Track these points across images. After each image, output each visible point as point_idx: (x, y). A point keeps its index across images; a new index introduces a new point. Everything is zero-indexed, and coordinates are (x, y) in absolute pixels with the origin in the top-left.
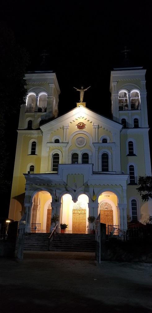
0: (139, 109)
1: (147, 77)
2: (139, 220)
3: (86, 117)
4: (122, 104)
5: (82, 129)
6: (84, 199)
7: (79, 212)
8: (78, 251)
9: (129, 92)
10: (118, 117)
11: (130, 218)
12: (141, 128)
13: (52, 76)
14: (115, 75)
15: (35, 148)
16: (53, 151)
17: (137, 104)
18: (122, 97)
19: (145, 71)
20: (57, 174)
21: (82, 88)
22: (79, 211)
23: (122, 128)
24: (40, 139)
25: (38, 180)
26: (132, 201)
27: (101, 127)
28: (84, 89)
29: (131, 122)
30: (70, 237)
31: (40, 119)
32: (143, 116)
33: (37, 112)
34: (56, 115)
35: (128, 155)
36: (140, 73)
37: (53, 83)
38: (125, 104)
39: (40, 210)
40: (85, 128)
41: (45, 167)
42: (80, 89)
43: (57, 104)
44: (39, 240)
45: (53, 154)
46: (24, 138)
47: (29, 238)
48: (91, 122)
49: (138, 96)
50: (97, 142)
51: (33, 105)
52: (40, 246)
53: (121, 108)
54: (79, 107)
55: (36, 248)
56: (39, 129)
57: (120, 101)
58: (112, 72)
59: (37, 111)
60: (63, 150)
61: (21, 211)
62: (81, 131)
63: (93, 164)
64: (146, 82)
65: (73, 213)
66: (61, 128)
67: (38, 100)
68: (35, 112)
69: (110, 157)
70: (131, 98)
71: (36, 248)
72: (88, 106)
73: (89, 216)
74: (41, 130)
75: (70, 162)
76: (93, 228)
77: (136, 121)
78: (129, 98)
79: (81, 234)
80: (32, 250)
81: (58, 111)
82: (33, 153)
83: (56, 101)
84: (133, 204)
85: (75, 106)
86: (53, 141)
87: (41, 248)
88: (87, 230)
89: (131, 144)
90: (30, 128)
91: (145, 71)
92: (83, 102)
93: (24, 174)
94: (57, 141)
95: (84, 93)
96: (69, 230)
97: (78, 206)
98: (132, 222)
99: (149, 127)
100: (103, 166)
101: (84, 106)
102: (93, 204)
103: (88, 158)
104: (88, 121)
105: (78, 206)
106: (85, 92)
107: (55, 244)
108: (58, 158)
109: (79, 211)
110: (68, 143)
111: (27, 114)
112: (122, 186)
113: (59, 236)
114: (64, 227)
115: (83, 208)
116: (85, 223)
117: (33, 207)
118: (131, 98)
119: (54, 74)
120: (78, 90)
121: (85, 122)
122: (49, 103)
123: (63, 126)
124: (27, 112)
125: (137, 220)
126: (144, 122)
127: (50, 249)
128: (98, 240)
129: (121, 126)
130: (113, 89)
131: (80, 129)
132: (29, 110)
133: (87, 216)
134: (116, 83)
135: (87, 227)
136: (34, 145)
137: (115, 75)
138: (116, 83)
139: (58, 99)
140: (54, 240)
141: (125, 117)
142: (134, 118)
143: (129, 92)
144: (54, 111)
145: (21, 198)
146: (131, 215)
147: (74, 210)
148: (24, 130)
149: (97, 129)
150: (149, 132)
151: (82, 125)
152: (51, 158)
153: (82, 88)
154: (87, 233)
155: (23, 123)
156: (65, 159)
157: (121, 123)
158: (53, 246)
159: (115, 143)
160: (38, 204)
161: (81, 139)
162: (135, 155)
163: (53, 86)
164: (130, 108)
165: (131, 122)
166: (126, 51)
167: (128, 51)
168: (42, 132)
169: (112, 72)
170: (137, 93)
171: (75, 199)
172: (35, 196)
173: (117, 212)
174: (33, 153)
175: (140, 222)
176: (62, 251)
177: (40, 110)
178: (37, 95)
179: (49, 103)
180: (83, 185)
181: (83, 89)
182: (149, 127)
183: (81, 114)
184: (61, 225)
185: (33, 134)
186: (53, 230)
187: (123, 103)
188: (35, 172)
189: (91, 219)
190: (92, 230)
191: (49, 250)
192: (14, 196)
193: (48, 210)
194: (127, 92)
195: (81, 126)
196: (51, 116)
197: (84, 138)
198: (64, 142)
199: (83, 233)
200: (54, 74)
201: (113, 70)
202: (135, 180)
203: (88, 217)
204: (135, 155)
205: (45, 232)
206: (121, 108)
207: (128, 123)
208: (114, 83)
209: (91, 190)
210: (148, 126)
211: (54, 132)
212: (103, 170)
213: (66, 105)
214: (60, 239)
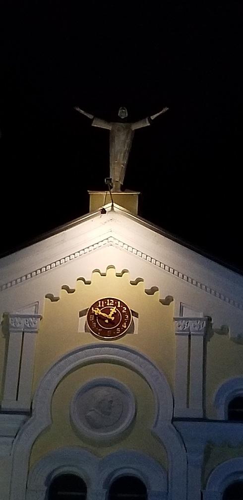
42: (112, 118)
121: (132, 298)
151: (113, 310)
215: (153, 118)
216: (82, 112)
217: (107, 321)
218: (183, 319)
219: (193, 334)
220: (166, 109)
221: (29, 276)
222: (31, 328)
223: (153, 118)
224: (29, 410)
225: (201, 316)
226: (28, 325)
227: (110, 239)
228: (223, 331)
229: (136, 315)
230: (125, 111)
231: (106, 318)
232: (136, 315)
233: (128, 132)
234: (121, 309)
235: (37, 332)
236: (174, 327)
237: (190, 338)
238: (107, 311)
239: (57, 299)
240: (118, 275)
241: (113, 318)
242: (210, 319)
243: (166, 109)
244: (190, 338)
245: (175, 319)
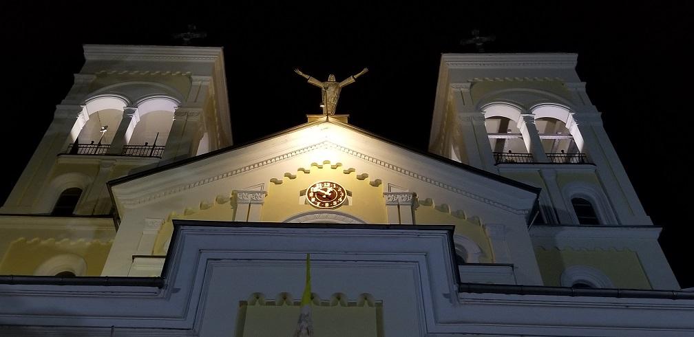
3: (348, 161)
13: (213, 56)
42: (323, 79)
58: (445, 57)
64: (587, 87)
66: (221, 201)
95: (337, 92)
106: (345, 92)
120: (313, 81)
121: (347, 183)
128: (88, 244)
150: (662, 240)
151: (330, 189)
159: (512, 266)
163: (205, 83)
169: (445, 57)
185: (70, 235)
215: (355, 77)
216: (301, 73)
217: (324, 196)
218: (391, 194)
219: (402, 204)
220: (365, 70)
221: (256, 166)
222: (257, 200)
223: (355, 77)
224: (500, 120)
225: (407, 191)
226: (254, 198)
227: (325, 143)
228: (427, 203)
229: (349, 194)
230: (333, 76)
231: (324, 194)
232: (349, 194)
233: (337, 88)
234: (337, 189)
235: (262, 204)
236: (385, 200)
237: (250, 205)
238: (326, 190)
239: (280, 183)
240: (334, 168)
241: (330, 194)
242: (414, 195)
243: (365, 70)
244: (250, 205)
245: (385, 194)
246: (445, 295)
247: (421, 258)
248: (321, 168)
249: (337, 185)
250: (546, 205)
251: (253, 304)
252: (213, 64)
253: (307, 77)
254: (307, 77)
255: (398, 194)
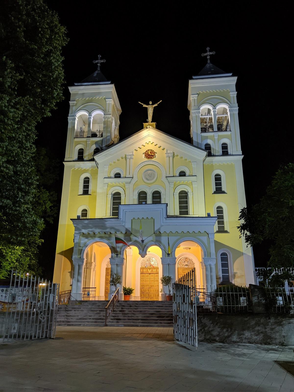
0: (228, 130)
1: (238, 86)
2: (232, 280)
4: (205, 124)
5: (151, 158)
6: (155, 252)
7: (150, 271)
8: (147, 326)
9: (214, 107)
10: (200, 141)
11: (220, 278)
12: (231, 155)
14: (195, 85)
15: (89, 185)
16: (113, 189)
17: (225, 124)
18: (205, 115)
19: (236, 78)
20: (118, 218)
21: (151, 103)
22: (150, 269)
23: (206, 157)
24: (95, 172)
25: (192, 376)
26: (215, 176)
27: (177, 156)
28: (153, 104)
29: (217, 148)
30: (136, 306)
31: (94, 147)
32: (233, 138)
33: (89, 137)
34: (116, 140)
35: (215, 193)
36: (228, 83)
37: (111, 98)
38: (209, 125)
39: (96, 269)
40: (155, 157)
41: (101, 209)
42: (148, 104)
43: (118, 127)
44: (92, 311)
45: (113, 193)
46: (73, 173)
47: (78, 308)
48: (163, 149)
49: (227, 113)
50: (173, 176)
51: (85, 129)
52: (93, 319)
53: (204, 130)
54: (147, 128)
55: (88, 322)
56: (93, 160)
57: (203, 121)
59: (90, 135)
60: (126, 187)
61: (70, 270)
62: (150, 161)
63: (167, 204)
64: (237, 94)
65: (142, 273)
67: (92, 121)
68: (87, 137)
69: (190, 196)
70: (217, 116)
71: (88, 322)
72: (159, 127)
73: (163, 276)
74: (96, 162)
75: (136, 202)
76: (168, 293)
77: (225, 147)
78: (215, 115)
79: (152, 302)
80: (82, 325)
81: (118, 137)
82: (86, 192)
83: (116, 123)
84: (222, 259)
85: (141, 128)
86: (113, 175)
87: (96, 322)
88: (160, 295)
89: (218, 178)
90: (81, 158)
91: (236, 78)
92: (152, 122)
93: (71, 219)
94: (118, 176)
96: (136, 296)
97: (148, 263)
98: (222, 284)
99: (243, 154)
100: (180, 208)
101: (154, 127)
102: (168, 257)
103: (160, 197)
104: (160, 147)
105: (148, 263)
107: (115, 316)
108: (120, 198)
109: (150, 269)
110: (133, 178)
111: (76, 140)
112: (208, 234)
113: (120, 304)
114: (128, 292)
115: (155, 266)
116: (158, 286)
117: (84, 264)
118: (217, 116)
119: (113, 86)
120: (145, 106)
122: (107, 125)
123: (125, 155)
124: (77, 137)
125: (229, 281)
126: (235, 147)
127: (108, 324)
129: (205, 153)
130: (193, 104)
131: (149, 158)
132: (80, 135)
133: (160, 275)
134: (197, 95)
135: (160, 291)
136: (87, 181)
137: (195, 85)
138: (197, 95)
139: (119, 120)
140: (114, 311)
141: (209, 142)
142: (222, 143)
143: (214, 107)
144: (113, 136)
145: (68, 254)
146: (221, 274)
147: (142, 268)
148: (74, 161)
149: (171, 158)
150: (243, 160)
152: (110, 197)
153: (151, 103)
154: (160, 299)
155: (71, 152)
156: (129, 198)
157: (204, 149)
158: (112, 319)
160: (93, 261)
161: (149, 172)
162: (224, 192)
164: (215, 129)
165: (217, 148)
166: (208, 53)
167: (211, 53)
168: (97, 164)
169: (190, 82)
170: (225, 110)
171: (143, 252)
172: (87, 250)
173: (201, 270)
174: (86, 192)
175: (233, 283)
176: (125, 326)
177: (94, 135)
178: (90, 114)
179: (107, 125)
180: (154, 233)
181: (151, 105)
182: (243, 154)
183: (149, 137)
184: (125, 289)
186: (113, 295)
187: (206, 123)
188: (89, 216)
189: (166, 280)
190: (167, 295)
191: (106, 325)
192: (60, 251)
193: (107, 269)
194: (211, 108)
195: (150, 155)
196: (110, 142)
197: (154, 171)
198: (127, 176)
199: (155, 299)
200: (113, 86)
201: (192, 79)
202: (228, 269)
203: (162, 276)
204: (224, 192)
205: (103, 299)
206: (204, 130)
207: (213, 149)
208: (194, 96)
209: (164, 239)
210: (241, 153)
211: (113, 164)
212: (181, 213)
213: (130, 125)
214: (122, 308)
215: (158, 103)
216: (140, 103)
221: (130, 145)
243: (161, 101)
245: (166, 153)
246: (165, 218)
247: (162, 210)
248: (148, 144)
249: (153, 150)
250: (213, 147)
251: (133, 219)
252: (112, 91)
253: (143, 104)
254: (143, 104)
255: (169, 153)
